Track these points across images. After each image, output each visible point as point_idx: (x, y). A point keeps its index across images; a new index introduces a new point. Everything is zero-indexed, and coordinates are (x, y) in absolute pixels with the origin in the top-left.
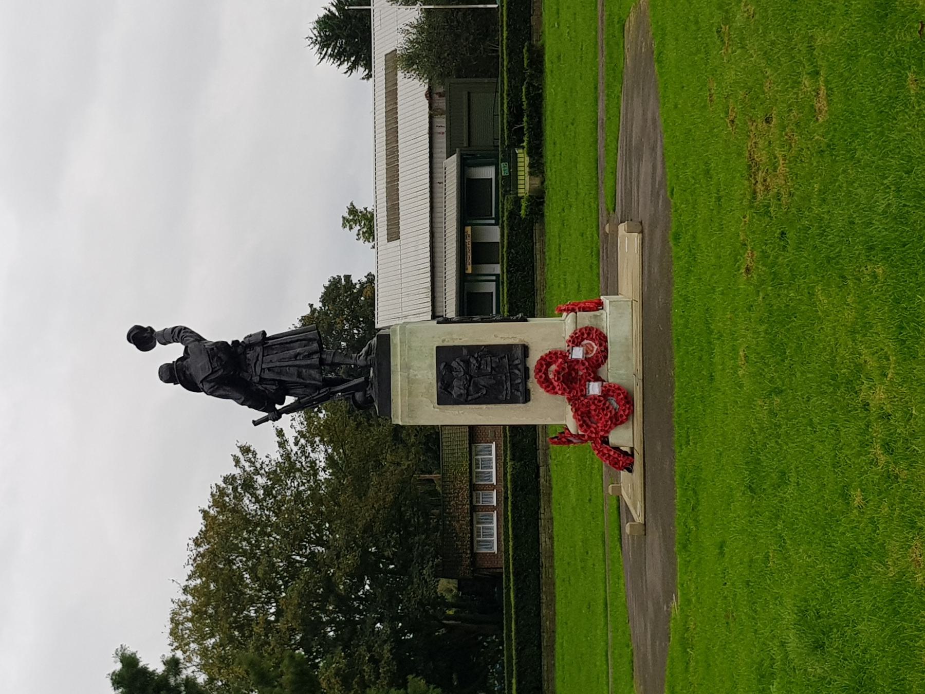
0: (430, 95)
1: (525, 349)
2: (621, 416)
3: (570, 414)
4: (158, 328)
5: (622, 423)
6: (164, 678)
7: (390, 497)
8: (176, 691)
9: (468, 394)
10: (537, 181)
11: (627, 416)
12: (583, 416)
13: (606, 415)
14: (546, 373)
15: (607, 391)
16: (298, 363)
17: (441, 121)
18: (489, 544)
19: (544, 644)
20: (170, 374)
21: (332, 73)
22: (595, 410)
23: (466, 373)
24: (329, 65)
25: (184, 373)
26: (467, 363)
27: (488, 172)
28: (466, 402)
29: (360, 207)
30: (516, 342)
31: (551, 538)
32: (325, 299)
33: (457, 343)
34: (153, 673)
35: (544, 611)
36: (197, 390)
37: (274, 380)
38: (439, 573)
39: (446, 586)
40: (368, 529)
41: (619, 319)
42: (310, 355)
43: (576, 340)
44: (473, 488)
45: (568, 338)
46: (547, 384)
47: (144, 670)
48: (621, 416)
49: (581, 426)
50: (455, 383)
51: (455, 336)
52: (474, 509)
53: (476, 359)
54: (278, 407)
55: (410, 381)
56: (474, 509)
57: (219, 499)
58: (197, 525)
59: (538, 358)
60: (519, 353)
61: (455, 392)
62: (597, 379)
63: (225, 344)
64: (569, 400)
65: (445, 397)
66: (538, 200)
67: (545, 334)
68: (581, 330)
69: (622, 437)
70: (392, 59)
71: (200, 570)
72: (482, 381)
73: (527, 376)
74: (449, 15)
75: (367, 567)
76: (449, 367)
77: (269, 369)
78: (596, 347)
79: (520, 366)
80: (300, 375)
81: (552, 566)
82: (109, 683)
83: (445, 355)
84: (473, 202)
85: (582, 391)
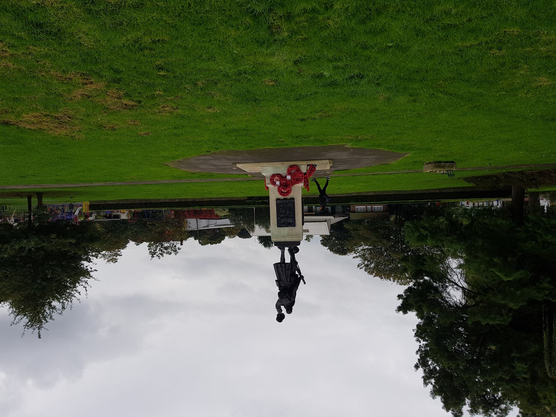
1: (278, 199)
4: (277, 313)
6: (404, 299)
8: (408, 297)
12: (297, 181)
15: (289, 173)
18: (381, 208)
20: (289, 311)
26: (282, 218)
28: (294, 217)
32: (326, 246)
36: (294, 301)
38: (388, 219)
39: (392, 218)
40: (377, 237)
41: (267, 170)
42: (282, 266)
43: (274, 183)
44: (367, 212)
46: (289, 192)
47: (402, 304)
52: (372, 211)
56: (372, 211)
57: (371, 273)
58: (378, 278)
60: (279, 201)
61: (291, 221)
62: (286, 177)
63: (279, 293)
65: (293, 224)
67: (274, 194)
69: (304, 169)
70: (268, 231)
71: (388, 278)
72: (288, 213)
73: (286, 199)
75: (388, 238)
76: (284, 223)
80: (288, 270)
82: (405, 315)
83: (280, 225)
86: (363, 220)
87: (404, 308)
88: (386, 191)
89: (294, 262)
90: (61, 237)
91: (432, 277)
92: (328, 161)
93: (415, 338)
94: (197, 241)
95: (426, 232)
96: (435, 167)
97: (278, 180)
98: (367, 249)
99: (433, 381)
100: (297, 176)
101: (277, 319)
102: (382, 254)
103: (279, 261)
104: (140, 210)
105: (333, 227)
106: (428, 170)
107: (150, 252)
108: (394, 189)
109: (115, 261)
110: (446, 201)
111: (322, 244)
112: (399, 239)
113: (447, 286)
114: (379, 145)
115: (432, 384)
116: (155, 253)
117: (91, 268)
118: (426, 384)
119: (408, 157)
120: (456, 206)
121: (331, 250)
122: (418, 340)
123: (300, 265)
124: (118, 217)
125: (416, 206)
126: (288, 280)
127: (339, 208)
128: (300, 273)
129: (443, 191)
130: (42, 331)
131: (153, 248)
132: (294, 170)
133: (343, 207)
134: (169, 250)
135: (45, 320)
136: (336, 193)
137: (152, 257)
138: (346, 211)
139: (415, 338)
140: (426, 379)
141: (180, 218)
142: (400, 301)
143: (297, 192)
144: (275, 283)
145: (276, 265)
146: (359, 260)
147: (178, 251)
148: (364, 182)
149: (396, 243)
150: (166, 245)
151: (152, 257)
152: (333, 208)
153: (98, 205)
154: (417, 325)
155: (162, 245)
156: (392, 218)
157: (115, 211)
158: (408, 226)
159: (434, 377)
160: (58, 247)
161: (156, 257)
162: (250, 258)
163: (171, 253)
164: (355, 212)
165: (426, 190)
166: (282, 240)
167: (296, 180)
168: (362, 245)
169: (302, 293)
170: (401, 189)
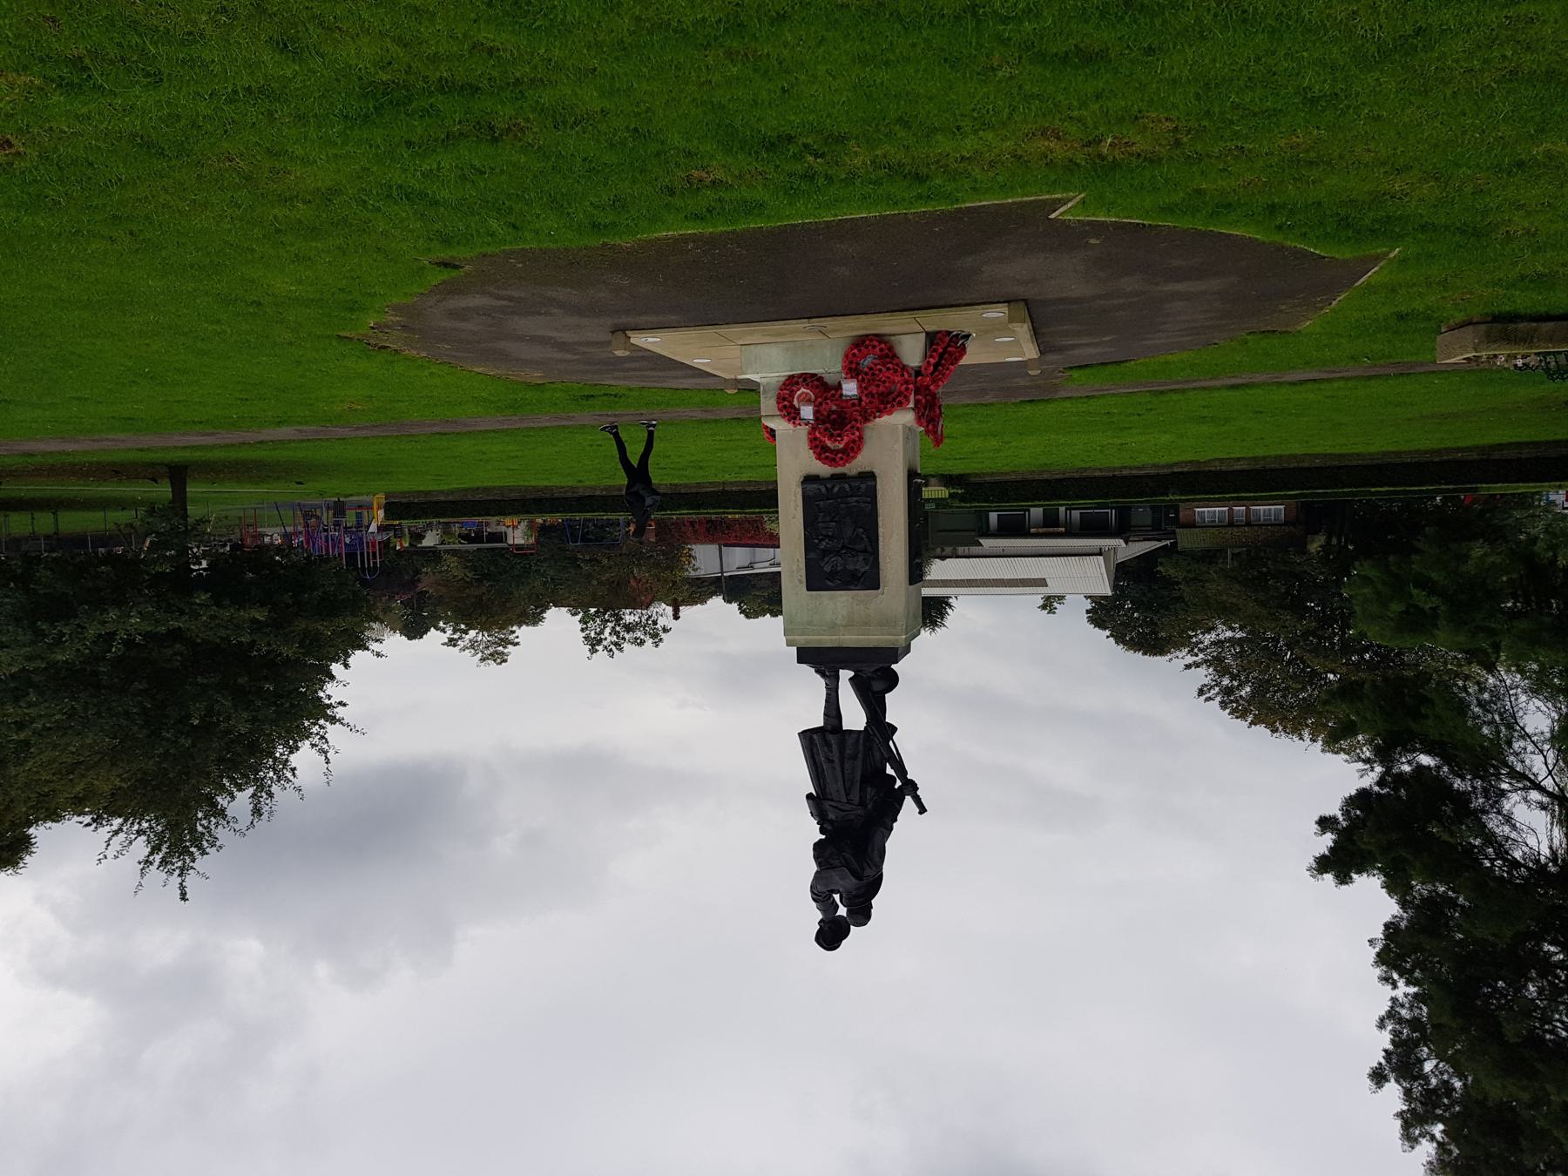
0: (943, 558)
5: (891, 349)
8: (1355, 824)
9: (865, 551)
10: (933, 480)
12: (886, 402)
15: (852, 370)
16: (836, 760)
17: (960, 550)
18: (1277, 513)
21: (952, 617)
23: (838, 553)
24: (947, 621)
25: (856, 896)
26: (825, 552)
27: (993, 517)
29: (1041, 602)
30: (799, 490)
31: (1238, 459)
33: (803, 566)
34: (1335, 842)
35: (1306, 465)
36: (881, 876)
37: (861, 789)
38: (1302, 550)
39: (1315, 545)
40: (1263, 604)
41: (763, 356)
42: (827, 744)
43: (792, 415)
44: (1231, 524)
45: (791, 426)
47: (1331, 849)
49: (900, 404)
50: (851, 567)
52: (1248, 524)
54: (898, 783)
55: (851, 624)
56: (1248, 524)
58: (1261, 730)
62: (839, 386)
63: (818, 847)
64: (867, 420)
65: (868, 579)
66: (948, 480)
67: (794, 459)
69: (912, 352)
71: (1295, 729)
76: (832, 575)
80: (854, 757)
81: (1264, 458)
82: (1344, 887)
83: (817, 580)
84: (1014, 528)
87: (1340, 863)
88: (1294, 457)
89: (879, 728)
90: (227, 602)
91: (1446, 758)
92: (1004, 308)
93: (1378, 972)
94: (735, 606)
95: (1435, 601)
96: (1490, 339)
97: (809, 401)
98: (1230, 640)
99: (1438, 1129)
101: (818, 939)
102: (1276, 656)
103: (819, 722)
104: (557, 518)
105: (1123, 573)
106: (1457, 352)
108: (1318, 450)
109: (500, 658)
110: (1499, 488)
111: (1091, 620)
112: (1332, 610)
113: (1503, 793)
114: (1224, 207)
115: (1433, 1138)
116: (600, 642)
117: (329, 697)
118: (1410, 1139)
119: (1370, 288)
120: (1531, 506)
121: (1119, 638)
122: (1386, 979)
123: (903, 742)
124: (500, 537)
125: (1396, 507)
126: (857, 797)
127: (1142, 514)
129: (1496, 455)
130: (191, 878)
131: (594, 626)
132: (869, 356)
134: (639, 634)
135: (200, 848)
136: (1117, 464)
137: (593, 651)
138: (1164, 523)
139: (1378, 972)
140: (1412, 1123)
141: (673, 545)
142: (1328, 839)
143: (889, 446)
144: (805, 808)
145: (807, 737)
146: (1203, 675)
147: (663, 636)
148: (1202, 420)
149: (1325, 621)
150: (629, 617)
151: (593, 651)
152: (1124, 513)
153: (409, 505)
154: (1387, 926)
155: (619, 619)
156: (1315, 545)
159: (1440, 1119)
160: (223, 633)
161: (601, 653)
162: (700, 706)
163: (642, 643)
164: (1192, 525)
166: (827, 640)
167: (881, 400)
168: (1213, 628)
169: (906, 840)
170: (1344, 451)
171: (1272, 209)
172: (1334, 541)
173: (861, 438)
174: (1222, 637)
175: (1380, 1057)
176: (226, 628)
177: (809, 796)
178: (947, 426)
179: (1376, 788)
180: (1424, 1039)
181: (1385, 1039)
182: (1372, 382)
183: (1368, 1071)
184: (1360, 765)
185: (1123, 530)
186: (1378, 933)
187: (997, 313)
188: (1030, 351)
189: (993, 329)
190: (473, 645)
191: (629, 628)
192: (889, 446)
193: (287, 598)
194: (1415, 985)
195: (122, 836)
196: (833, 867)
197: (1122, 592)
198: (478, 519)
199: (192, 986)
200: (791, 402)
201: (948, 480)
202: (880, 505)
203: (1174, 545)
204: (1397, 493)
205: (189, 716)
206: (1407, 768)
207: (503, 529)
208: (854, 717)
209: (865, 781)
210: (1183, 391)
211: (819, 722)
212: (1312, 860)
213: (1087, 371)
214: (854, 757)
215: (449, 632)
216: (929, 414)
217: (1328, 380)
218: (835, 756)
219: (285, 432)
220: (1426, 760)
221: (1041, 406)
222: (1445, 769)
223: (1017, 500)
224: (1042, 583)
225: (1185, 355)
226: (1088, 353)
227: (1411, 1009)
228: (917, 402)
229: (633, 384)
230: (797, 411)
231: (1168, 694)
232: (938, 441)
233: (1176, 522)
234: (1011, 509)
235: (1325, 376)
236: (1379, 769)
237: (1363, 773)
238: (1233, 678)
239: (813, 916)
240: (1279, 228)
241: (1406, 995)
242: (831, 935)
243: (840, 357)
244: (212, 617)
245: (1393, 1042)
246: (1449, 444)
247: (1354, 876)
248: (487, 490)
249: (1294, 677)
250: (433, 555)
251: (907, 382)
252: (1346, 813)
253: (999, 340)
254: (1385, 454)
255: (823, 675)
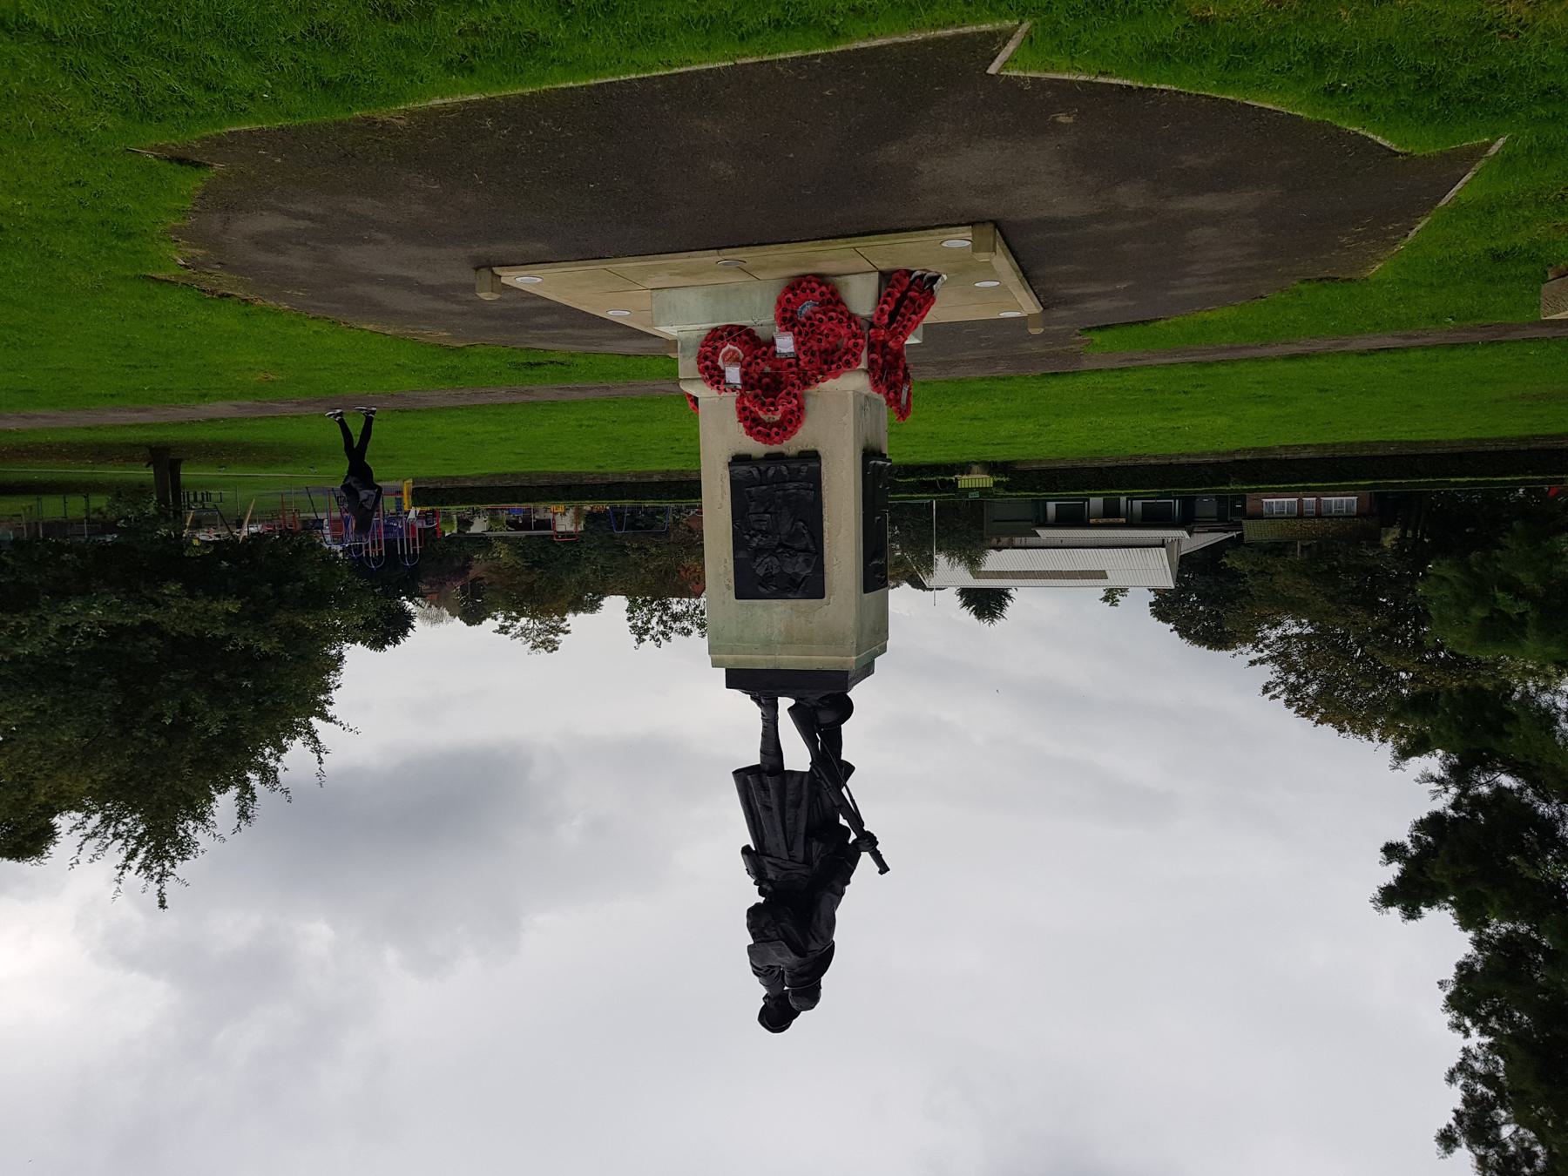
0: (999, 549)
2: (822, 294)
3: (830, 384)
7: (1305, 581)
8: (1426, 852)
9: (806, 550)
10: (976, 468)
11: (820, 284)
12: (831, 361)
13: (821, 320)
14: (778, 424)
16: (775, 807)
17: (1017, 541)
18: (1349, 504)
19: (1413, 451)
21: (1011, 609)
22: (820, 341)
23: (773, 553)
26: (759, 551)
27: (1051, 506)
29: (1103, 594)
30: (727, 473)
31: (1305, 447)
34: (1403, 872)
38: (1375, 542)
39: (1389, 539)
40: (1332, 599)
41: (679, 301)
43: (714, 377)
44: (1301, 516)
45: (715, 392)
46: (793, 420)
47: (1398, 880)
48: (822, 294)
49: (848, 364)
50: (789, 570)
51: (721, 570)
52: (1319, 516)
53: (753, 536)
54: (853, 836)
55: (789, 641)
56: (1319, 516)
58: (1328, 729)
59: (751, 440)
60: (743, 469)
62: (772, 343)
64: (806, 385)
65: (811, 586)
66: (992, 467)
67: (720, 434)
68: (701, 371)
69: (862, 297)
71: (1364, 730)
74: (940, 536)
76: (766, 580)
77: (789, 849)
78: (729, 346)
79: (762, 468)
81: (1334, 445)
82: (1411, 922)
83: (748, 585)
84: (1073, 518)
85: (790, 365)
86: (1292, 543)
87: (1408, 894)
88: (1367, 444)
89: (831, 766)
90: (200, 593)
91: (1533, 782)
92: (967, 232)
95: (1522, 606)
97: (735, 360)
100: (823, 331)
102: (1346, 653)
103: (756, 760)
104: (605, 505)
105: (1186, 565)
107: (634, 627)
108: (1394, 436)
109: (552, 646)
116: (647, 631)
119: (1459, 208)
121: (1183, 631)
122: (1457, 1026)
123: (857, 788)
124: (546, 524)
126: (804, 851)
127: (1207, 505)
128: (856, 820)
130: (170, 885)
132: (810, 298)
133: (1221, 499)
134: (686, 624)
136: (1173, 450)
137: (640, 640)
138: (1230, 513)
139: (1449, 1017)
142: (1395, 869)
143: (839, 419)
144: (740, 864)
145: (743, 777)
146: (1268, 672)
149: (1398, 618)
150: (677, 606)
151: (640, 640)
152: (1188, 503)
153: (436, 490)
154: (1460, 966)
155: (666, 608)
156: (1389, 539)
157: (541, 506)
158: (1444, 579)
160: (198, 625)
161: (649, 643)
163: (689, 633)
164: (1259, 516)
165: (1521, 439)
166: (760, 660)
168: (1280, 624)
171: (1319, 57)
172: (1409, 534)
173: (801, 408)
174: (1289, 633)
175: (1450, 1118)
176: (202, 621)
177: (746, 850)
178: (916, 389)
179: (1450, 812)
180: (1501, 1100)
181: (1454, 1097)
182: (1457, 353)
183: (1435, 1133)
184: (1433, 786)
185: (1187, 521)
186: (1450, 973)
187: (958, 241)
188: (1024, 304)
189: (965, 269)
190: (524, 632)
191: (676, 618)
192: (839, 419)
193: (267, 588)
194: (1490, 1035)
195: (96, 841)
196: (768, 940)
197: (1188, 584)
198: (524, 506)
199: (264, 970)
200: (714, 362)
201: (992, 467)
202: (825, 493)
203: (1241, 536)
204: (1479, 484)
205: (162, 715)
206: (1485, 790)
207: (550, 516)
208: (797, 755)
209: (811, 833)
210: (1233, 362)
211: (756, 760)
212: (1376, 891)
213: (1109, 334)
214: (797, 805)
215: (501, 619)
216: (890, 374)
217: (1405, 350)
218: (773, 801)
219: (220, 408)
220: (1506, 781)
221: (1069, 380)
222: (1529, 791)
223: (1066, 489)
224: (1102, 575)
225: (1227, 313)
226: (1101, 307)
227: (1486, 1061)
228: (871, 362)
229: (574, 348)
230: (722, 373)
231: (1234, 687)
232: (903, 413)
233: (1243, 513)
234: (1071, 498)
235: (1398, 342)
236: (1453, 790)
237: (1435, 795)
238: (1299, 676)
239: (756, 993)
240: (1331, 91)
241: (1480, 1046)
242: (776, 1016)
243: (774, 301)
244: (186, 609)
245: (1464, 1101)
246: (1539, 431)
247: (1424, 910)
248: (514, 475)
249: (1364, 675)
250: (483, 542)
251: (855, 336)
252: (1416, 840)
253: (981, 289)
254: (1468, 441)
255: (759, 704)
